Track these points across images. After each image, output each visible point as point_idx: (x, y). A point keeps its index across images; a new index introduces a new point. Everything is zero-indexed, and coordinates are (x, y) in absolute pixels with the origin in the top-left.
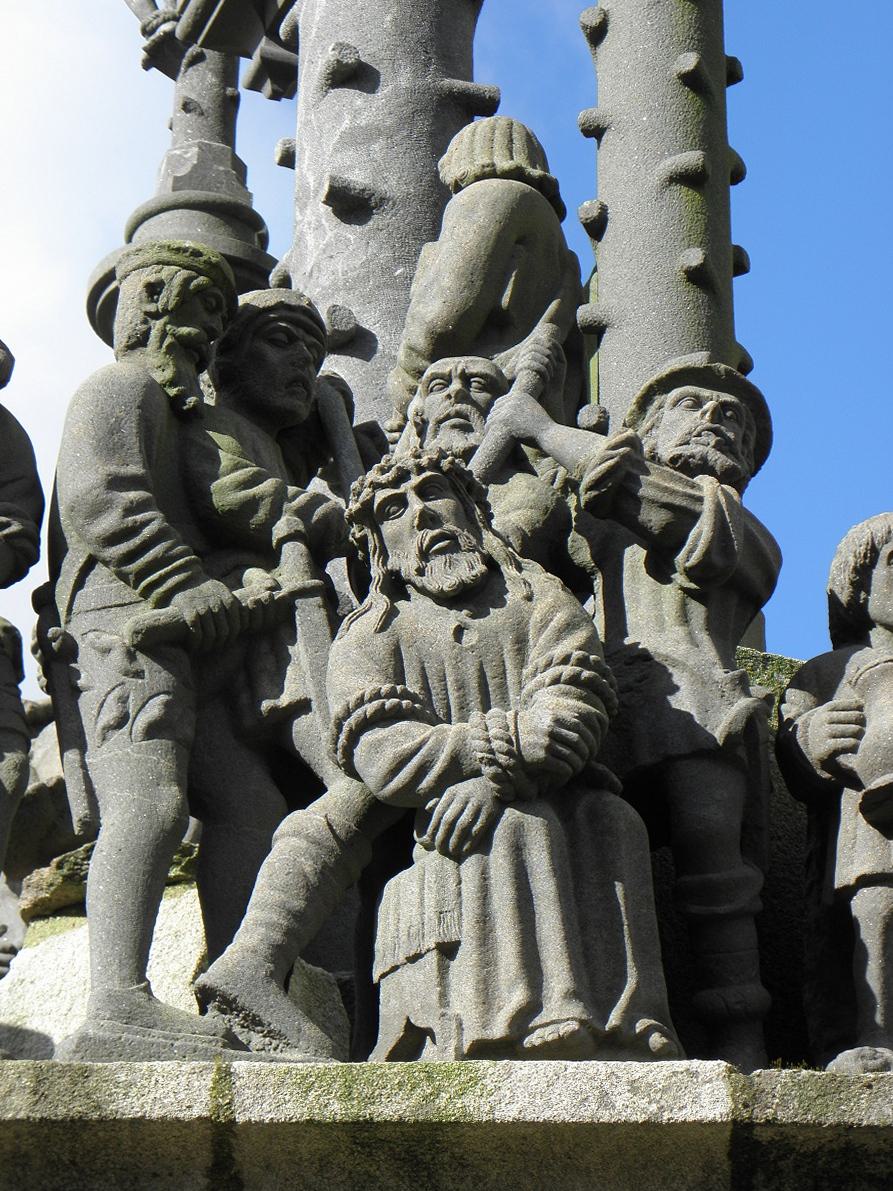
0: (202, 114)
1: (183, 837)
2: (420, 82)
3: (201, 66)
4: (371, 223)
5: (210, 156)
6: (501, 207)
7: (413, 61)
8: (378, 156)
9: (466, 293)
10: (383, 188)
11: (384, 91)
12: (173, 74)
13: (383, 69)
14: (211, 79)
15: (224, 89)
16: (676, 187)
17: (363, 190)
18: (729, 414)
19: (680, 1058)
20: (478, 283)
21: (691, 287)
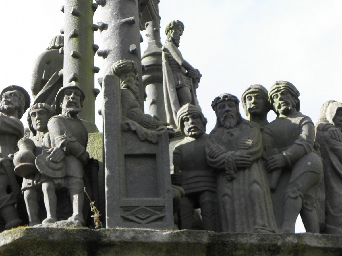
0: (149, 36)
1: (91, 210)
2: (116, 23)
3: (148, 26)
4: (108, 57)
5: (151, 44)
6: (40, 58)
7: (114, 19)
8: (108, 42)
9: (35, 79)
10: (110, 48)
11: (109, 28)
12: (145, 29)
13: (109, 24)
14: (151, 28)
15: (154, 28)
16: (71, 39)
17: (105, 51)
18: (12, 95)
19: (341, 162)
20: (37, 76)
21: (74, 59)
